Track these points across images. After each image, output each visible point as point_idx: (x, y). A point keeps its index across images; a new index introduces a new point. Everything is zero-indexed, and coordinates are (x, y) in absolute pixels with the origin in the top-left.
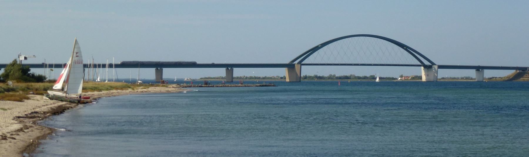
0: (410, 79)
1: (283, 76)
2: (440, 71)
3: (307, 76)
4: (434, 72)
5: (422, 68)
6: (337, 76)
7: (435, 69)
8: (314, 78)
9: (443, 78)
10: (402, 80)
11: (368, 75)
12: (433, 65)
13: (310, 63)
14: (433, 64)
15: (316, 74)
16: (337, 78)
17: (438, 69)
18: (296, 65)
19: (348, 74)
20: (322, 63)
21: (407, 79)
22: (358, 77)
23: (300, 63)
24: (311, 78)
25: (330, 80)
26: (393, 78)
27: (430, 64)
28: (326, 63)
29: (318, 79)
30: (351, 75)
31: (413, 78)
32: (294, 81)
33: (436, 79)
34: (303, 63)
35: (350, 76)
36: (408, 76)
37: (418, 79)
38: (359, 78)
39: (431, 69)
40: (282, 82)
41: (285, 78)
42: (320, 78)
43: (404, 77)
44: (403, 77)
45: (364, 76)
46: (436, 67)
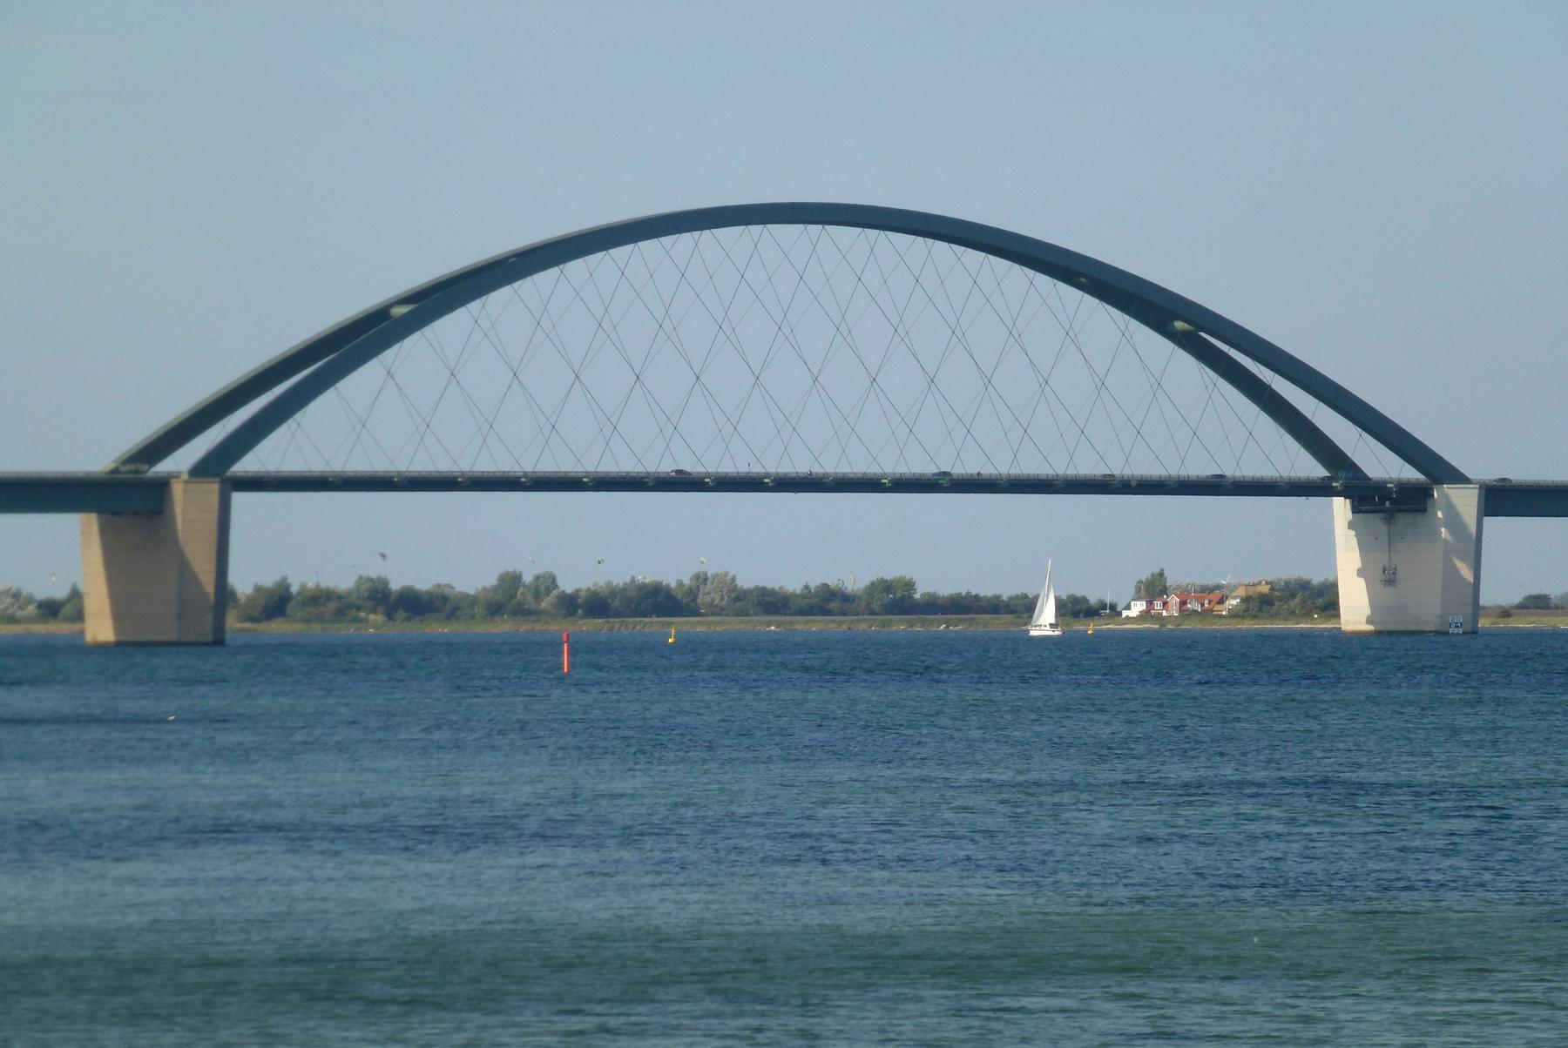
0: (1234, 615)
1: (60, 593)
2: (1503, 531)
3: (294, 589)
4: (1445, 541)
5: (1341, 507)
6: (567, 585)
7: (1454, 520)
8: (359, 608)
9: (1538, 603)
10: (1159, 618)
11: (855, 580)
12: (1438, 481)
13: (313, 464)
14: (1439, 471)
15: (375, 570)
16: (570, 605)
17: (1487, 520)
18: (177, 490)
19: (673, 573)
20: (422, 465)
21: (1207, 614)
22: (763, 592)
23: (213, 466)
24: (333, 606)
25: (502, 628)
26: (1085, 599)
27: (1411, 474)
28: (712, 469)
29: (390, 616)
30: (701, 579)
31: (1260, 603)
32: (166, 638)
33: (1469, 610)
34: (248, 464)
35: (693, 593)
36: (1218, 587)
37: (1307, 614)
38: (771, 603)
39: (1420, 518)
40: (48, 650)
41: (79, 616)
42: (414, 604)
43: (1174, 600)
44: (1165, 591)
45: (814, 584)
46: (1465, 500)
